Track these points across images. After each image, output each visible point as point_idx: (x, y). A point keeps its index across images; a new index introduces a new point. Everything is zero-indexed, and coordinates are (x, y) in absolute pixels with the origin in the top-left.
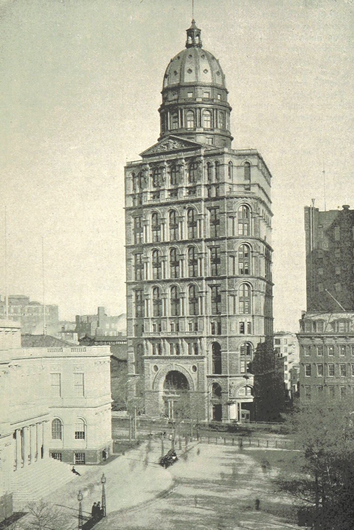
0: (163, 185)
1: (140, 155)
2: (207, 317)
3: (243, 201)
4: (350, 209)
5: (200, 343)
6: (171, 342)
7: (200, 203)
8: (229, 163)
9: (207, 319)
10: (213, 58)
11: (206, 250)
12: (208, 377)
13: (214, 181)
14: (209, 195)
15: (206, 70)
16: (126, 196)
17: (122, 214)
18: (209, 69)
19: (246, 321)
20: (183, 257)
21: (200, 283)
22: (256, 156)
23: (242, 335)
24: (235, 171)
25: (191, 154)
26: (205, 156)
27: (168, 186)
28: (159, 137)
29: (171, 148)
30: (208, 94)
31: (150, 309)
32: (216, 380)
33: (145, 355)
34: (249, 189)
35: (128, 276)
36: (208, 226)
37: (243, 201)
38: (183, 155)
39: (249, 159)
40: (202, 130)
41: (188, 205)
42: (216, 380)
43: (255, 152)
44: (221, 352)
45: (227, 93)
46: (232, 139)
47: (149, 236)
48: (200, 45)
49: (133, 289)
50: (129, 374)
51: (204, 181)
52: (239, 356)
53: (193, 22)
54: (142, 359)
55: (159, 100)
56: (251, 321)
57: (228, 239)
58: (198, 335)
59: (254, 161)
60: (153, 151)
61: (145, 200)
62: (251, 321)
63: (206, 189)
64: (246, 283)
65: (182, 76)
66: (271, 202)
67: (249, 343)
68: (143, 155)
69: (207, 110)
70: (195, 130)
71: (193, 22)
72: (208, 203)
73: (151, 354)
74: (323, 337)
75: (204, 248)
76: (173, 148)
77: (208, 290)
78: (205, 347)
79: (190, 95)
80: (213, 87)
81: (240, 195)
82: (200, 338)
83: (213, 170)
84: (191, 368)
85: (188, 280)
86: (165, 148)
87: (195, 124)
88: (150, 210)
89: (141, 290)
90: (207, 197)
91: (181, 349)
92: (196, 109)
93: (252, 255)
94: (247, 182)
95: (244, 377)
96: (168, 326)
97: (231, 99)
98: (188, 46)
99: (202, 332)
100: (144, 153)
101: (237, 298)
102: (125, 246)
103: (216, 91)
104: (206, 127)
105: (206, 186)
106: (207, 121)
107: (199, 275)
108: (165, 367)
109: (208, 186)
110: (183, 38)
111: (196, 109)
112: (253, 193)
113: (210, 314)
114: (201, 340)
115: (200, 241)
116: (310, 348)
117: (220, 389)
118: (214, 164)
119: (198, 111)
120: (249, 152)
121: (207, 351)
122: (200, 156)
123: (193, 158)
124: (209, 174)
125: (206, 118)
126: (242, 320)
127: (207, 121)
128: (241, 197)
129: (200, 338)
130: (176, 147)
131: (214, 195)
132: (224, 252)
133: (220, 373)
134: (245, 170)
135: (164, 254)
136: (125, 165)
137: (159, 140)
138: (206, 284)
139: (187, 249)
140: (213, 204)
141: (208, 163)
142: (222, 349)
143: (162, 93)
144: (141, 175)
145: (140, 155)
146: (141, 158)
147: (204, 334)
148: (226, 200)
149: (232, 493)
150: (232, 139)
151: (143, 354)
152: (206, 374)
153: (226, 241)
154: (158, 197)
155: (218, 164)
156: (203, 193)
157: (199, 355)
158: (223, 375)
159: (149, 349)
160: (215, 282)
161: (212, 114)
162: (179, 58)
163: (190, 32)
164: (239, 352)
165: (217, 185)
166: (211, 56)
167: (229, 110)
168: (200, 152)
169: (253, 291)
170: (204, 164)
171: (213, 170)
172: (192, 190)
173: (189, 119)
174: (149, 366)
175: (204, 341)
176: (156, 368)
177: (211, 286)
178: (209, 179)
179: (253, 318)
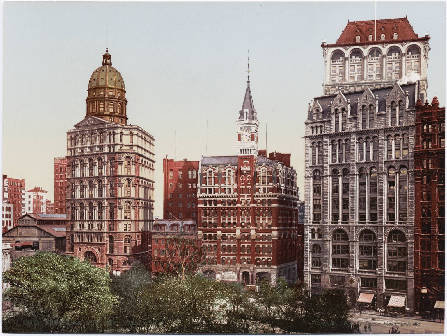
0: (86, 144)
2: (107, 221)
4: (187, 161)
6: (79, 234)
10: (117, 72)
13: (112, 143)
16: (68, 149)
23: (125, 231)
24: (124, 137)
27: (88, 144)
28: (86, 115)
34: (132, 148)
40: (108, 113)
48: (110, 64)
51: (107, 142)
52: (123, 243)
53: (107, 51)
55: (86, 95)
58: (102, 231)
66: (153, 154)
67: (369, 222)
68: (77, 126)
71: (107, 51)
78: (105, 239)
79: (102, 93)
81: (127, 151)
83: (112, 136)
90: (108, 151)
91: (93, 239)
94: (131, 144)
97: (127, 96)
98: (103, 64)
99: (103, 229)
104: (110, 111)
106: (111, 108)
108: (84, 249)
109: (109, 146)
110: (101, 60)
112: (134, 150)
114: (103, 234)
116: (157, 240)
121: (107, 240)
122: (105, 128)
124: (110, 139)
125: (110, 106)
127: (111, 108)
132: (117, 184)
133: (113, 253)
134: (131, 137)
136: (67, 131)
137: (85, 117)
141: (110, 133)
142: (114, 239)
143: (88, 91)
146: (75, 128)
147: (105, 231)
149: (395, 322)
156: (106, 150)
157: (102, 242)
158: (114, 254)
160: (111, 201)
162: (97, 71)
164: (123, 241)
165: (114, 146)
166: (115, 71)
167: (125, 103)
171: (112, 136)
172: (101, 147)
173: (101, 106)
174: (76, 248)
178: (110, 142)
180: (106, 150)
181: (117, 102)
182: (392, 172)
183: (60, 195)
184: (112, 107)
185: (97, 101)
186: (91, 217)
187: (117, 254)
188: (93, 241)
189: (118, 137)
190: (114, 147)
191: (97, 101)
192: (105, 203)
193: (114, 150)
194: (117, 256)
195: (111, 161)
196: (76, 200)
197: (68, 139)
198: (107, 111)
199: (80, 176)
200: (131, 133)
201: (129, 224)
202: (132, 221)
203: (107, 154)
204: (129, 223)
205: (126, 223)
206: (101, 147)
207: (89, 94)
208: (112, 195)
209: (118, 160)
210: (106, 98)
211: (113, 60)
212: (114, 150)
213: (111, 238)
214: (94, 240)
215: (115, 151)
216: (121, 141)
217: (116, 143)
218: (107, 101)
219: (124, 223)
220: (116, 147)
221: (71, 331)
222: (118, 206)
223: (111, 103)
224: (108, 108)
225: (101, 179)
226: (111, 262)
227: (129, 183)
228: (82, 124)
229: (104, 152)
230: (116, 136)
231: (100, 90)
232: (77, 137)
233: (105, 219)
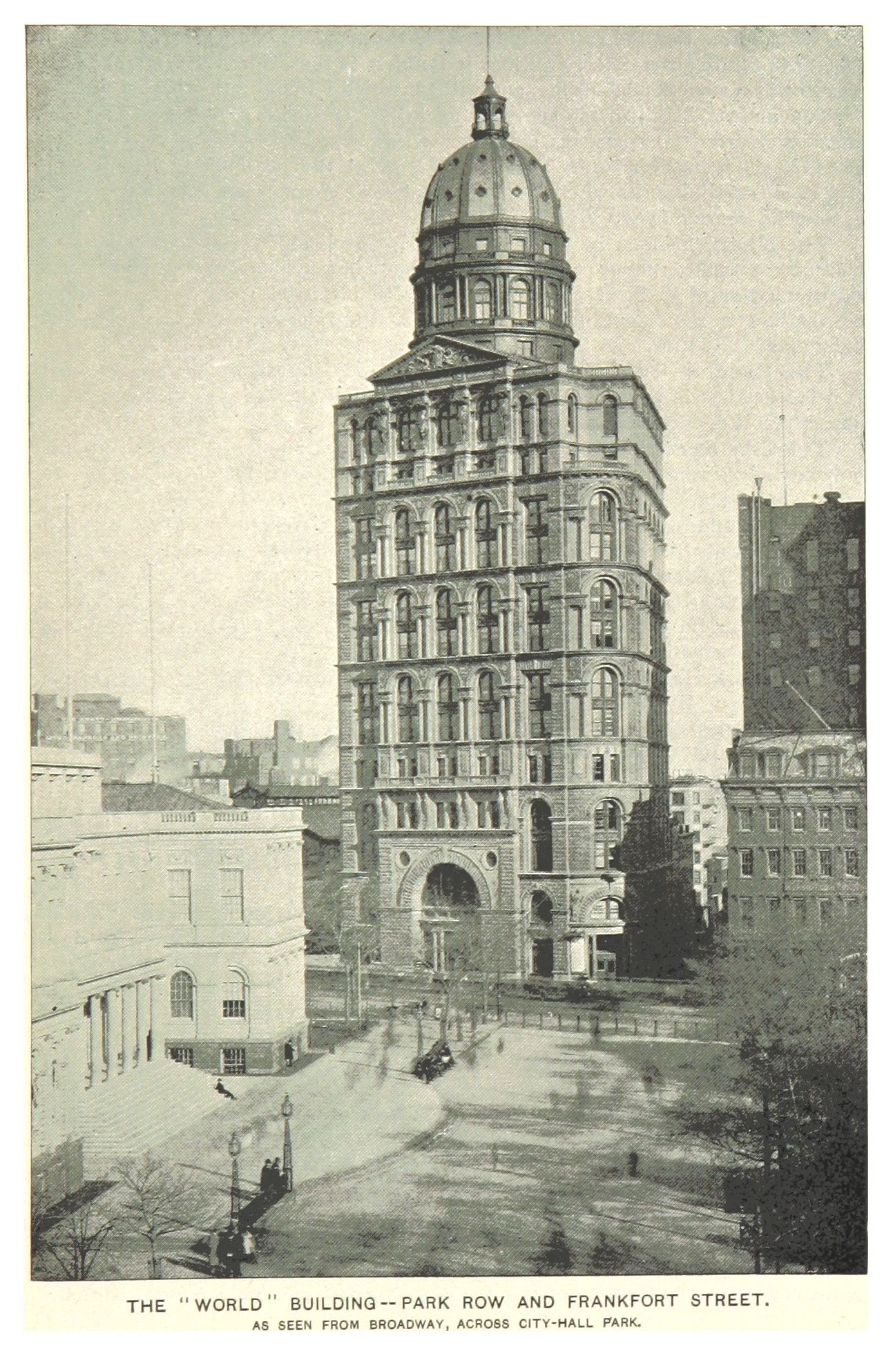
0: (421, 447)
1: (369, 379)
2: (519, 743)
3: (601, 482)
4: (840, 500)
5: (505, 801)
8: (570, 397)
9: (520, 747)
10: (534, 162)
11: (517, 593)
12: (522, 877)
13: (536, 438)
15: (517, 189)
17: (329, 511)
18: (523, 186)
19: (607, 752)
21: (504, 668)
23: (598, 783)
24: (582, 415)
25: (484, 377)
26: (515, 382)
28: (412, 338)
29: (439, 364)
30: (521, 243)
31: (392, 724)
32: (539, 885)
33: (381, 829)
34: (614, 456)
35: (341, 568)
37: (601, 482)
38: (466, 380)
39: (615, 389)
40: (507, 324)
42: (539, 885)
45: (565, 240)
46: (576, 343)
47: (389, 562)
48: (503, 134)
49: (354, 681)
50: (345, 871)
51: (514, 437)
53: (489, 82)
54: (374, 838)
55: (412, 257)
56: (619, 751)
57: (566, 568)
58: (500, 783)
59: (625, 393)
60: (399, 372)
61: (381, 480)
62: (619, 751)
65: (463, 203)
66: (663, 486)
68: (377, 380)
69: (520, 280)
70: (492, 322)
71: (489, 82)
72: (521, 487)
73: (393, 827)
74: (779, 789)
75: (512, 588)
76: (444, 363)
78: (515, 812)
79: (482, 246)
82: (505, 790)
84: (485, 858)
86: (425, 364)
87: (493, 310)
88: (392, 503)
89: (372, 683)
90: (519, 474)
91: (461, 814)
92: (495, 275)
93: (621, 603)
94: (610, 440)
95: (604, 877)
96: (431, 763)
97: (573, 255)
98: (477, 134)
99: (508, 778)
100: (377, 375)
102: (333, 499)
103: (540, 236)
106: (520, 303)
107: (502, 648)
108: (425, 856)
109: (523, 450)
110: (467, 117)
112: (624, 465)
113: (526, 736)
116: (750, 812)
117: (549, 904)
118: (535, 400)
120: (613, 372)
121: (521, 820)
122: (505, 381)
123: (489, 386)
125: (517, 297)
126: (598, 749)
127: (520, 303)
129: (505, 790)
130: (449, 362)
131: (535, 470)
132: (558, 598)
133: (550, 869)
135: (423, 602)
136: (336, 402)
137: (411, 345)
140: (533, 489)
142: (554, 816)
143: (418, 240)
144: (370, 424)
145: (369, 379)
146: (371, 387)
147: (514, 782)
148: (562, 482)
150: (576, 343)
151: (375, 826)
152: (518, 872)
153: (562, 572)
154: (410, 475)
156: (511, 465)
157: (502, 828)
158: (555, 873)
162: (456, 161)
163: (481, 104)
164: (592, 823)
165: (542, 448)
166: (528, 158)
169: (622, 685)
170: (514, 399)
171: (534, 413)
172: (486, 458)
173: (478, 298)
174: (391, 852)
175: (514, 796)
176: (405, 858)
177: (530, 674)
178: (525, 434)
179: (624, 746)
181: (541, 277)
182: (65, 680)
186: (410, 734)
188: (503, 818)
194: (568, 881)
196: (380, 665)
207: (425, 254)
208: (539, 640)
210: (500, 263)
214: (467, 818)
222: (569, 685)
228: (391, 375)
229: (500, 474)
231: (474, 233)
233: (513, 737)
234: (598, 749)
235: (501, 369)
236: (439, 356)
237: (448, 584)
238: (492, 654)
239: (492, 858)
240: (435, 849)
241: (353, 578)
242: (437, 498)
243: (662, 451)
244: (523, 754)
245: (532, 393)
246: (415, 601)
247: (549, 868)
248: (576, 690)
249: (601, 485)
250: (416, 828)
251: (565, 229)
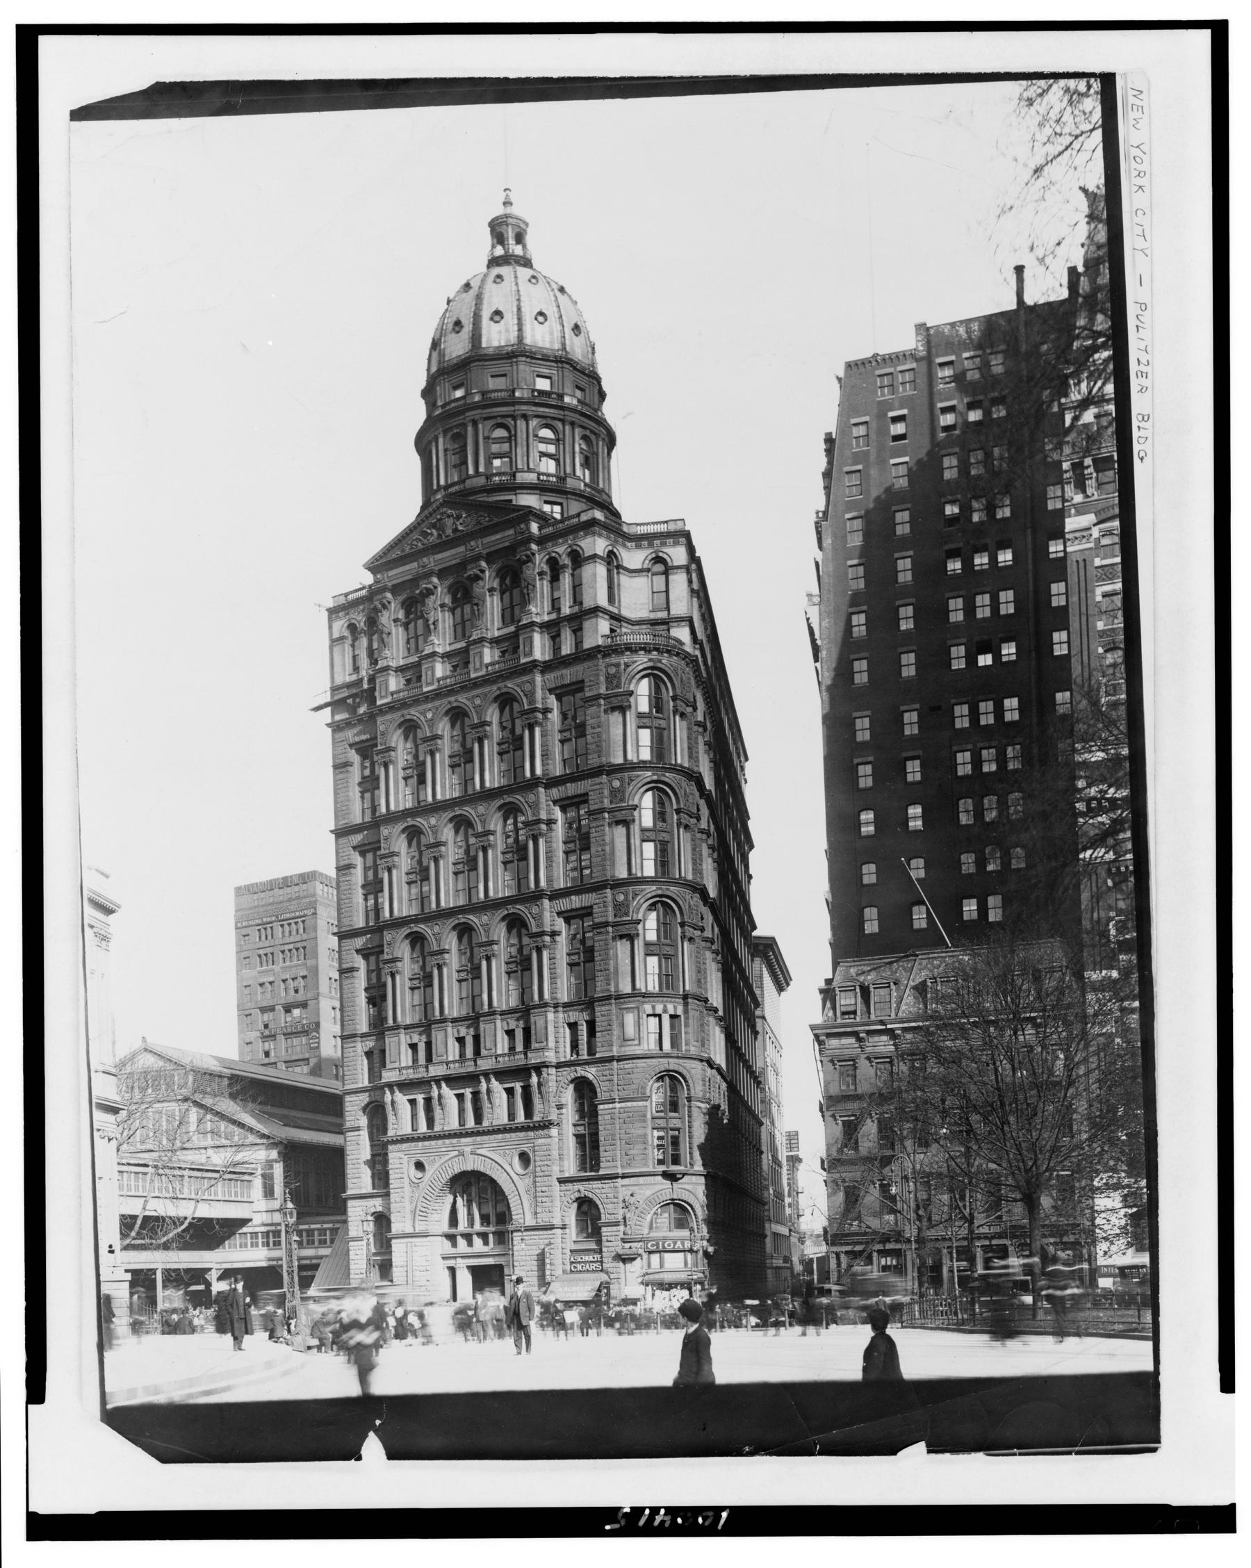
3: (650, 660)
5: (540, 1084)
7: (528, 677)
8: (608, 556)
9: (556, 1012)
11: (549, 813)
12: (562, 1181)
14: (556, 649)
15: (541, 314)
19: (665, 1011)
20: (489, 840)
21: (531, 797)
22: (683, 540)
26: (541, 541)
29: (449, 532)
30: (548, 381)
31: (405, 1005)
35: (340, 809)
36: (563, 969)
37: (650, 660)
38: (480, 545)
41: (499, 689)
43: (679, 526)
44: (600, 1228)
47: (399, 796)
51: (539, 611)
53: (507, 203)
54: (384, 1145)
55: (417, 414)
56: (680, 1011)
57: (613, 887)
58: (534, 1059)
59: (678, 555)
60: (403, 551)
61: (383, 694)
62: (680, 1011)
63: (546, 636)
64: (664, 899)
68: (377, 565)
72: (550, 676)
73: (406, 1129)
74: (892, 1030)
75: (543, 805)
76: (455, 530)
77: (556, 928)
80: (562, 362)
82: (538, 1068)
84: (516, 1160)
85: (504, 902)
86: (432, 534)
88: (396, 717)
89: (379, 950)
93: (683, 933)
95: (666, 1175)
101: (635, 829)
102: (331, 831)
103: (569, 375)
105: (545, 626)
107: (536, 997)
109: (552, 629)
110: (483, 245)
111: (514, 418)
113: (564, 998)
114: (539, 1074)
115: (538, 896)
118: (566, 560)
119: (521, 424)
120: (662, 528)
123: (512, 549)
126: (654, 1007)
128: (644, 649)
129: (538, 1068)
130: (460, 528)
131: (567, 649)
135: (432, 732)
138: (551, 912)
139: (503, 926)
141: (554, 565)
144: (372, 622)
147: (550, 1057)
148: (615, 1063)
151: (385, 1131)
153: (615, 1063)
154: (419, 678)
155: (578, 559)
156: (540, 648)
159: (402, 1119)
161: (561, 436)
163: (498, 230)
168: (528, 529)
170: (540, 562)
172: (511, 644)
174: (400, 1161)
175: (551, 1075)
177: (568, 916)
179: (686, 1004)
180: (540, 648)
181: (572, 424)
183: (264, 1010)
184: (551, 449)
185: (475, 423)
187: (620, 1171)
189: (597, 574)
190: (577, 631)
191: (475, 423)
192: (548, 916)
193: (578, 643)
195: (559, 698)
197: (334, 642)
198: (529, 470)
199: (409, 805)
200: (658, 560)
201: (672, 1017)
202: (685, 997)
203: (547, 667)
204: (671, 1011)
205: (659, 1009)
206: (511, 644)
209: (603, 690)
211: (535, 245)
212: (578, 643)
213: (584, 1089)
215: (588, 644)
216: (611, 599)
217: (588, 603)
218: (525, 417)
219: (648, 1008)
220: (587, 625)
221: (1046, 307)
223: (546, 433)
224: (534, 455)
225: (518, 798)
226: (588, 1210)
227: (662, 803)
230: (587, 570)
232: (385, 619)
234: (654, 1007)
235: (523, 526)
236: (449, 522)
237: (462, 699)
238: (522, 785)
239: (525, 1158)
240: (456, 1153)
241: (357, 819)
242: (450, 703)
243: (756, 1033)
244: (561, 1020)
245: (561, 549)
246: (429, 838)
247: (596, 1166)
248: (623, 930)
249: (650, 664)
250: (433, 1129)
251: (601, 371)
